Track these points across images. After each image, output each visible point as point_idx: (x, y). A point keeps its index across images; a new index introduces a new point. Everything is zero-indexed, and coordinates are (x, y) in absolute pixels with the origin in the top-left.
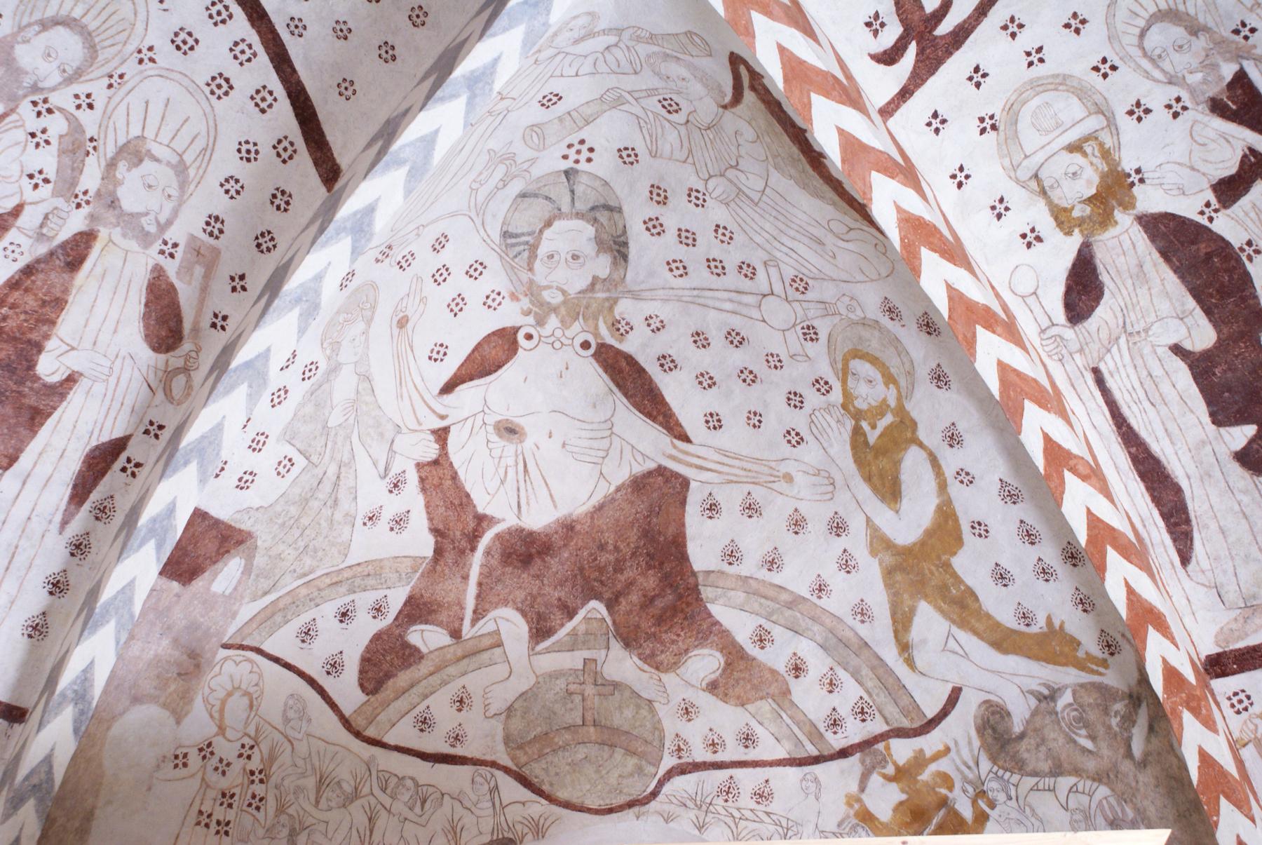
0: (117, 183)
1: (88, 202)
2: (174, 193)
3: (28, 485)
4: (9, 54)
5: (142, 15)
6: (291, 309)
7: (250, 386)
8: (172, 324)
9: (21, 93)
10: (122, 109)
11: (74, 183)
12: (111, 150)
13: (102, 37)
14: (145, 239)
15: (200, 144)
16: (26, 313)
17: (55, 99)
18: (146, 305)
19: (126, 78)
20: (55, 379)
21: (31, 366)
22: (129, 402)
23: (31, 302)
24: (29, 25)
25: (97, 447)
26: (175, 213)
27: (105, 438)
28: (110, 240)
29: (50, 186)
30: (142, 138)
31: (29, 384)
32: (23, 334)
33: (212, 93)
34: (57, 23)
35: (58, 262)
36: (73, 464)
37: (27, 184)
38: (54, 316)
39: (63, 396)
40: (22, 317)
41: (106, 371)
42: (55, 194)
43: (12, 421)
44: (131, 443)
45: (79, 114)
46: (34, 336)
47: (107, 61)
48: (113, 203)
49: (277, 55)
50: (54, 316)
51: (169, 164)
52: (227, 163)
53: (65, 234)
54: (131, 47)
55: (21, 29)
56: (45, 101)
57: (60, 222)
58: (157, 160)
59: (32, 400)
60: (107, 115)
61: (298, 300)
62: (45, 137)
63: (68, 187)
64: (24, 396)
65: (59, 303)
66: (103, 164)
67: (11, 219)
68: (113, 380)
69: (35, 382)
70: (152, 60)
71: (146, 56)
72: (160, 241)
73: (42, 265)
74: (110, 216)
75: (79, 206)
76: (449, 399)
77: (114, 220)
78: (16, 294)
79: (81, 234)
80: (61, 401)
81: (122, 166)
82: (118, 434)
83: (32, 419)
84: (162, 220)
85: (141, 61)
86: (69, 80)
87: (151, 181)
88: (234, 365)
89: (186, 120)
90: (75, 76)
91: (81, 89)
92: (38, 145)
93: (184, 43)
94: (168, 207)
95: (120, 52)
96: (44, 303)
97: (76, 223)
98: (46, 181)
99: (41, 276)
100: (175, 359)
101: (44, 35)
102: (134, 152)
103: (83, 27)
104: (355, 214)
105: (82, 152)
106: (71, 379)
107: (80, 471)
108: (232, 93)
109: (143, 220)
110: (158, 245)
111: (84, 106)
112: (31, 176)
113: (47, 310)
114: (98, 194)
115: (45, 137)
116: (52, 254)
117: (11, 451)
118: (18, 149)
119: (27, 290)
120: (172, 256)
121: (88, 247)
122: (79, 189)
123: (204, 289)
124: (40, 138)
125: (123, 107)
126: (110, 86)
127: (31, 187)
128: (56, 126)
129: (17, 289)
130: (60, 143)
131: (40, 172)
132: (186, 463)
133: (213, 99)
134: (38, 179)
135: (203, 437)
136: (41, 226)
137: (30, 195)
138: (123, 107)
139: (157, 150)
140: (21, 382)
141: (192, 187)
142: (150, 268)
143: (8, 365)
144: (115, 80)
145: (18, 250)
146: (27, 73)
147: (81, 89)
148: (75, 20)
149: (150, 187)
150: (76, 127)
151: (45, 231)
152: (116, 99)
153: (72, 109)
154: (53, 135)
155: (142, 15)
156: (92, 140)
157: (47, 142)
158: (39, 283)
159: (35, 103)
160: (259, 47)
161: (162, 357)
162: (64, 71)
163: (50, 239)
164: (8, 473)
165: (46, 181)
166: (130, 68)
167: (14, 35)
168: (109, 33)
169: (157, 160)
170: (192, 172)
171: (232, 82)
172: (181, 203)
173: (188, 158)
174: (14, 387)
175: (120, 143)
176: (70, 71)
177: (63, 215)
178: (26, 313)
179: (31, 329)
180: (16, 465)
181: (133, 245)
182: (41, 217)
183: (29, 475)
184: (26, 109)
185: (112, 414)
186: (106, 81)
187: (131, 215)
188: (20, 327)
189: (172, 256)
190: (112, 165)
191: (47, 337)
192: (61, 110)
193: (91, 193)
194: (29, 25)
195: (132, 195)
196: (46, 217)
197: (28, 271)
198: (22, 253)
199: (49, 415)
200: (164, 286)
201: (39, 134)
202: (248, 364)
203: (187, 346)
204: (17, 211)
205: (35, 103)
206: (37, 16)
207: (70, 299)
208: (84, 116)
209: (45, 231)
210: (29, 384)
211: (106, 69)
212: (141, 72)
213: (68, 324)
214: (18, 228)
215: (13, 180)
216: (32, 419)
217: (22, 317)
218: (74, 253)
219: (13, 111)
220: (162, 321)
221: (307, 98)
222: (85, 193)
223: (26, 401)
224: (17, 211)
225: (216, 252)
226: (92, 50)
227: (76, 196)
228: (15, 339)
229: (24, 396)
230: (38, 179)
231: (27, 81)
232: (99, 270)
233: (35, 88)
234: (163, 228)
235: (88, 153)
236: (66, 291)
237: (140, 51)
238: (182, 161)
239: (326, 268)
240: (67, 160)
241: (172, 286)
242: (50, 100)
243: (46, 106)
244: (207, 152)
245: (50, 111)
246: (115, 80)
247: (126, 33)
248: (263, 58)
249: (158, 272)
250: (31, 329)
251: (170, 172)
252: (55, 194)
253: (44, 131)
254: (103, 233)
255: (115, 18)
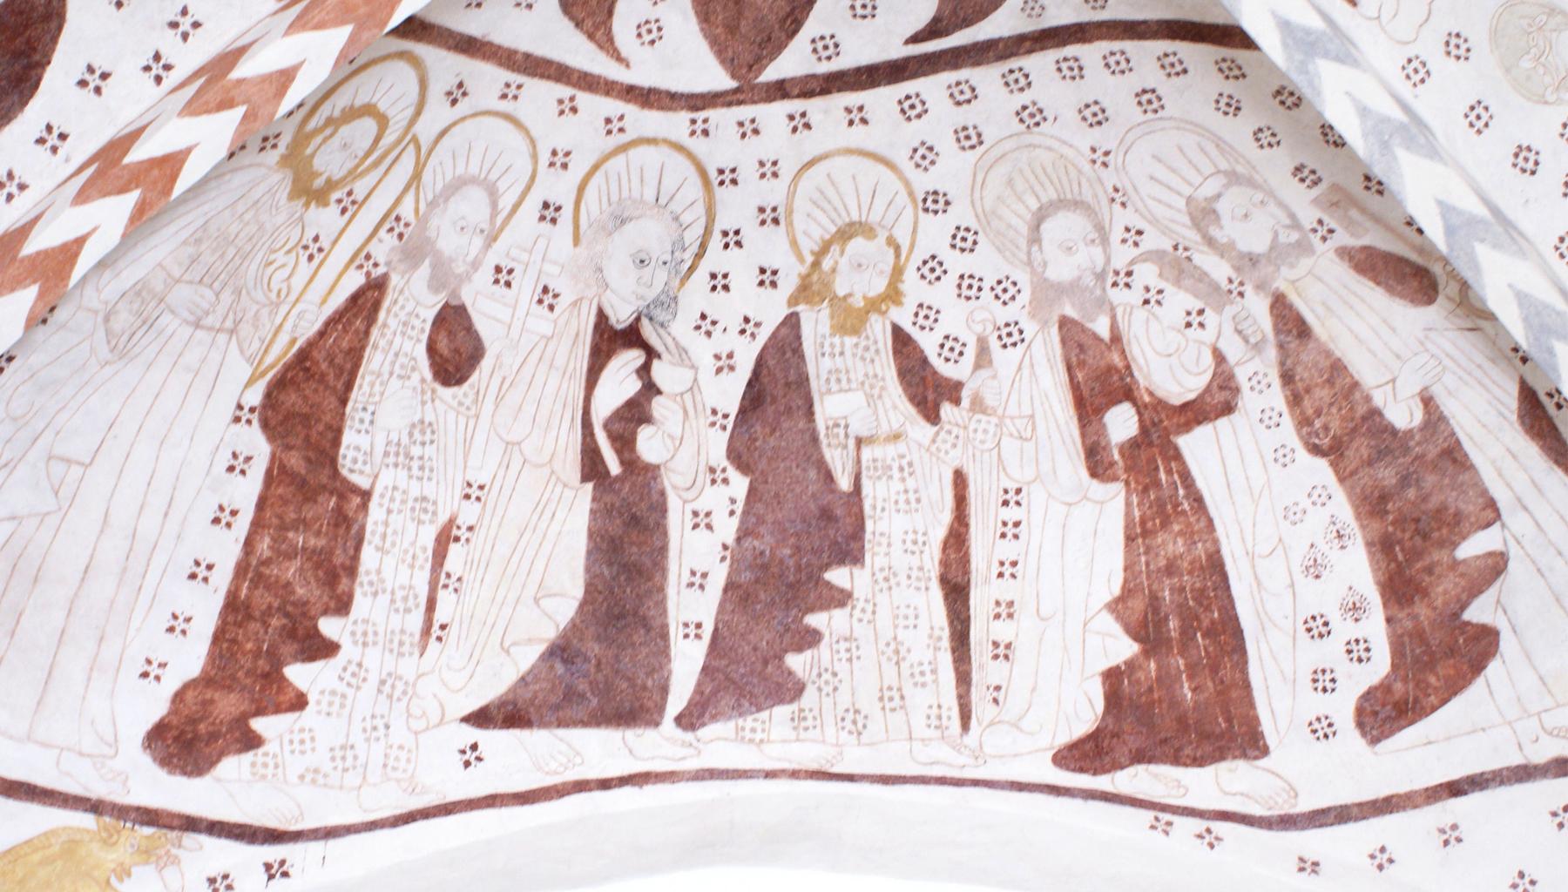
0: (1231, 245)
1: (1241, 284)
2: (1259, 196)
3: (1531, 507)
4: (1052, 286)
5: (1056, 145)
6: (1395, 158)
7: (1482, 241)
8: (1408, 270)
9: (1098, 292)
10: (1152, 204)
11: (1216, 287)
12: (1192, 236)
13: (1068, 191)
14: (1303, 247)
15: (1211, 148)
16: (1331, 404)
17: (1120, 263)
18: (1378, 284)
19: (1119, 186)
20: (1419, 417)
21: (1394, 432)
22: (1480, 359)
23: (1323, 394)
24: (1029, 253)
25: (1521, 417)
26: (1281, 204)
27: (1514, 404)
28: (1293, 282)
29: (1208, 312)
30: (1189, 200)
31: (1412, 443)
32: (1352, 419)
33: (1156, 111)
34: (1038, 226)
35: (1292, 346)
36: (1530, 451)
37: (1193, 332)
38: (1348, 380)
39: (1442, 418)
40: (1334, 410)
41: (1433, 362)
42: (1219, 309)
43: (1447, 481)
44: (1531, 381)
45: (1144, 247)
46: (1361, 410)
47: (1095, 196)
48: (1253, 260)
49: (1125, 31)
50: (1348, 380)
51: (1227, 186)
52: (1239, 131)
53: (1266, 323)
54: (1087, 167)
55: (1029, 263)
56: (1117, 273)
57: (1250, 321)
58: (1219, 196)
59: (1433, 452)
60: (1154, 221)
61: (1385, 146)
62: (1153, 292)
63: (1219, 296)
64: (1423, 455)
65: (1337, 368)
66: (1205, 249)
67: (1224, 366)
68: (1446, 361)
69: (1412, 437)
70: (1107, 153)
71: (1101, 158)
72: (1311, 236)
73: (1289, 362)
74: (1265, 270)
75: (1241, 294)
76: (886, 342)
77: (1271, 269)
78: (1307, 402)
79: (1272, 307)
80: (1448, 423)
81: (1213, 231)
82: (1514, 390)
83: (1455, 461)
84: (1288, 222)
85: (1105, 164)
86: (1104, 240)
87: (1240, 212)
88: (1442, 247)
89: (1181, 150)
90: (1102, 235)
91: (1117, 234)
92: (1159, 303)
93: (1095, 116)
94: (1272, 207)
95: (1088, 180)
96: (1330, 382)
97: (1258, 308)
98: (1201, 312)
99: (1299, 369)
100: (1448, 289)
101: (1045, 243)
102: (1203, 215)
103: (1051, 204)
104: (1285, 45)
105: (1185, 264)
106: (1428, 401)
107: (1542, 447)
108: (1159, 92)
109: (1282, 239)
110: (1315, 240)
111: (1137, 238)
112: (1189, 325)
113: (1339, 383)
114: (1238, 269)
115: (1153, 292)
116: (1281, 346)
117: (1480, 500)
118: (1153, 323)
119: (1308, 390)
120: (1331, 231)
121: (1290, 307)
122: (1224, 285)
123: (1377, 220)
124: (1152, 296)
125: (1150, 203)
126: (1123, 204)
127: (1199, 330)
128: (1147, 274)
129: (1302, 399)
130: (1167, 280)
131: (1189, 313)
132: (1551, 352)
133: (1160, 113)
134: (1195, 320)
135: (1526, 320)
136: (1246, 341)
137: (1208, 335)
138: (1150, 203)
139: (1209, 189)
140: (1406, 450)
141: (1257, 177)
142: (1337, 260)
143: (1380, 452)
144: (1120, 199)
145: (1260, 377)
146: (1080, 278)
147: (1117, 234)
148: (1040, 209)
149: (1246, 216)
150: (1156, 256)
151: (1253, 340)
152: (1140, 205)
153: (1136, 252)
154: (1155, 283)
155: (1056, 145)
156: (1176, 248)
157: (1160, 292)
158: (1306, 375)
159: (1115, 284)
160: (1117, 45)
161: (1441, 299)
162: (1093, 241)
163: (1264, 339)
164: (1504, 517)
165: (1201, 312)
166: (1110, 178)
167: (1033, 272)
168: (1065, 180)
169: (1219, 196)
170: (1239, 169)
171: (1148, 87)
172: (1271, 193)
173: (1224, 165)
174: (1408, 459)
175: (1186, 220)
176: (1094, 235)
177: (1244, 314)
178: (1331, 404)
179: (1351, 409)
180: (1501, 505)
181: (1305, 263)
182: (1237, 338)
183: (1519, 500)
184: (1117, 296)
185: (1486, 381)
186: (1117, 207)
187: (1272, 248)
188: (1343, 419)
189: (1331, 231)
190: (1210, 242)
191: (1368, 399)
192: (1132, 262)
193: (1234, 276)
194: (1029, 253)
195: (1253, 239)
196: (1239, 332)
197: (1287, 378)
198: (1265, 375)
199: (1458, 442)
200: (1363, 257)
201: (1147, 296)
202: (1450, 231)
203: (1437, 269)
204: (1219, 357)
205: (1115, 284)
206: (1023, 243)
207: (1338, 354)
208: (1148, 243)
209: (1253, 340)
210: (1412, 443)
211: (1105, 202)
212: (1116, 169)
213: (1365, 370)
214: (1237, 364)
215: (1183, 343)
216: (1455, 461)
217: (1334, 410)
218: (1290, 324)
219: (1113, 309)
220: (1401, 278)
221: (1177, 22)
222: (1231, 281)
223: (1430, 456)
224: (1219, 357)
225: (1335, 188)
226: (1077, 204)
227: (1230, 292)
228: (1354, 430)
229: (1423, 455)
230: (1195, 320)
231: (1089, 280)
232: (1320, 310)
233: (1100, 277)
234: (1295, 225)
235: (1189, 259)
236: (1328, 354)
237: (1094, 162)
238: (1225, 173)
239: (1354, 100)
240: (1188, 282)
241: (1365, 248)
242: (1118, 268)
243: (1122, 274)
244: (1219, 143)
245: (1129, 274)
246: (1120, 199)
247: (1070, 168)
248: (1130, 46)
249: (1345, 253)
250: (1351, 409)
251: (1235, 190)
252: (1219, 309)
253: (1147, 290)
254: (1281, 285)
255: (1050, 170)
